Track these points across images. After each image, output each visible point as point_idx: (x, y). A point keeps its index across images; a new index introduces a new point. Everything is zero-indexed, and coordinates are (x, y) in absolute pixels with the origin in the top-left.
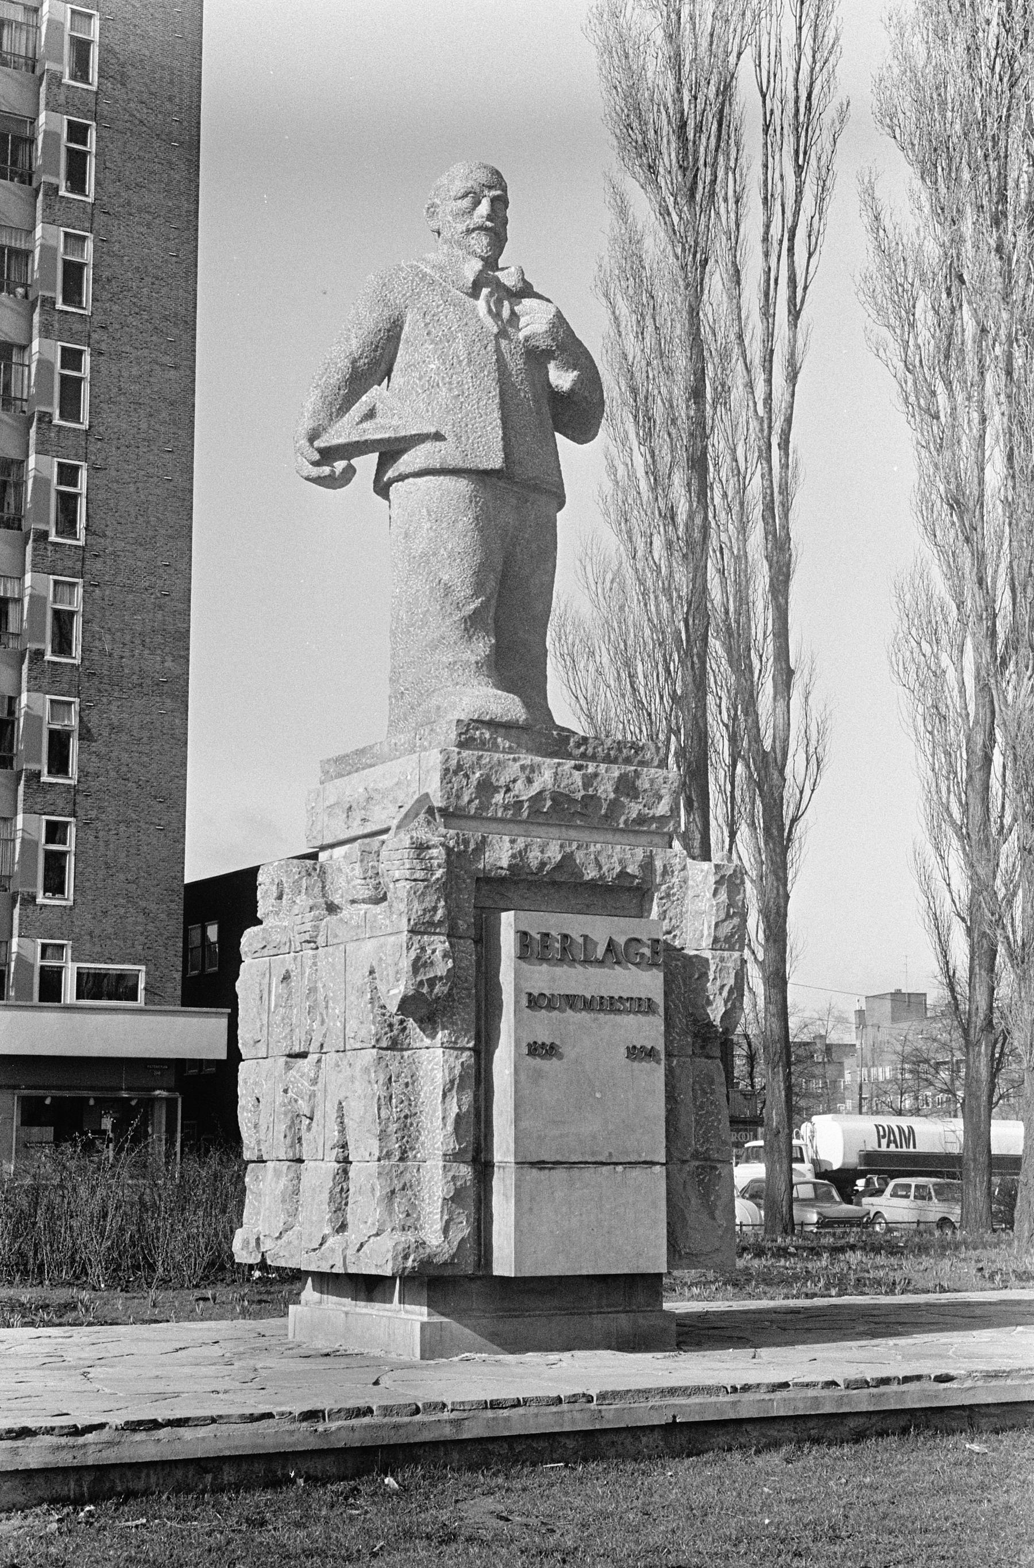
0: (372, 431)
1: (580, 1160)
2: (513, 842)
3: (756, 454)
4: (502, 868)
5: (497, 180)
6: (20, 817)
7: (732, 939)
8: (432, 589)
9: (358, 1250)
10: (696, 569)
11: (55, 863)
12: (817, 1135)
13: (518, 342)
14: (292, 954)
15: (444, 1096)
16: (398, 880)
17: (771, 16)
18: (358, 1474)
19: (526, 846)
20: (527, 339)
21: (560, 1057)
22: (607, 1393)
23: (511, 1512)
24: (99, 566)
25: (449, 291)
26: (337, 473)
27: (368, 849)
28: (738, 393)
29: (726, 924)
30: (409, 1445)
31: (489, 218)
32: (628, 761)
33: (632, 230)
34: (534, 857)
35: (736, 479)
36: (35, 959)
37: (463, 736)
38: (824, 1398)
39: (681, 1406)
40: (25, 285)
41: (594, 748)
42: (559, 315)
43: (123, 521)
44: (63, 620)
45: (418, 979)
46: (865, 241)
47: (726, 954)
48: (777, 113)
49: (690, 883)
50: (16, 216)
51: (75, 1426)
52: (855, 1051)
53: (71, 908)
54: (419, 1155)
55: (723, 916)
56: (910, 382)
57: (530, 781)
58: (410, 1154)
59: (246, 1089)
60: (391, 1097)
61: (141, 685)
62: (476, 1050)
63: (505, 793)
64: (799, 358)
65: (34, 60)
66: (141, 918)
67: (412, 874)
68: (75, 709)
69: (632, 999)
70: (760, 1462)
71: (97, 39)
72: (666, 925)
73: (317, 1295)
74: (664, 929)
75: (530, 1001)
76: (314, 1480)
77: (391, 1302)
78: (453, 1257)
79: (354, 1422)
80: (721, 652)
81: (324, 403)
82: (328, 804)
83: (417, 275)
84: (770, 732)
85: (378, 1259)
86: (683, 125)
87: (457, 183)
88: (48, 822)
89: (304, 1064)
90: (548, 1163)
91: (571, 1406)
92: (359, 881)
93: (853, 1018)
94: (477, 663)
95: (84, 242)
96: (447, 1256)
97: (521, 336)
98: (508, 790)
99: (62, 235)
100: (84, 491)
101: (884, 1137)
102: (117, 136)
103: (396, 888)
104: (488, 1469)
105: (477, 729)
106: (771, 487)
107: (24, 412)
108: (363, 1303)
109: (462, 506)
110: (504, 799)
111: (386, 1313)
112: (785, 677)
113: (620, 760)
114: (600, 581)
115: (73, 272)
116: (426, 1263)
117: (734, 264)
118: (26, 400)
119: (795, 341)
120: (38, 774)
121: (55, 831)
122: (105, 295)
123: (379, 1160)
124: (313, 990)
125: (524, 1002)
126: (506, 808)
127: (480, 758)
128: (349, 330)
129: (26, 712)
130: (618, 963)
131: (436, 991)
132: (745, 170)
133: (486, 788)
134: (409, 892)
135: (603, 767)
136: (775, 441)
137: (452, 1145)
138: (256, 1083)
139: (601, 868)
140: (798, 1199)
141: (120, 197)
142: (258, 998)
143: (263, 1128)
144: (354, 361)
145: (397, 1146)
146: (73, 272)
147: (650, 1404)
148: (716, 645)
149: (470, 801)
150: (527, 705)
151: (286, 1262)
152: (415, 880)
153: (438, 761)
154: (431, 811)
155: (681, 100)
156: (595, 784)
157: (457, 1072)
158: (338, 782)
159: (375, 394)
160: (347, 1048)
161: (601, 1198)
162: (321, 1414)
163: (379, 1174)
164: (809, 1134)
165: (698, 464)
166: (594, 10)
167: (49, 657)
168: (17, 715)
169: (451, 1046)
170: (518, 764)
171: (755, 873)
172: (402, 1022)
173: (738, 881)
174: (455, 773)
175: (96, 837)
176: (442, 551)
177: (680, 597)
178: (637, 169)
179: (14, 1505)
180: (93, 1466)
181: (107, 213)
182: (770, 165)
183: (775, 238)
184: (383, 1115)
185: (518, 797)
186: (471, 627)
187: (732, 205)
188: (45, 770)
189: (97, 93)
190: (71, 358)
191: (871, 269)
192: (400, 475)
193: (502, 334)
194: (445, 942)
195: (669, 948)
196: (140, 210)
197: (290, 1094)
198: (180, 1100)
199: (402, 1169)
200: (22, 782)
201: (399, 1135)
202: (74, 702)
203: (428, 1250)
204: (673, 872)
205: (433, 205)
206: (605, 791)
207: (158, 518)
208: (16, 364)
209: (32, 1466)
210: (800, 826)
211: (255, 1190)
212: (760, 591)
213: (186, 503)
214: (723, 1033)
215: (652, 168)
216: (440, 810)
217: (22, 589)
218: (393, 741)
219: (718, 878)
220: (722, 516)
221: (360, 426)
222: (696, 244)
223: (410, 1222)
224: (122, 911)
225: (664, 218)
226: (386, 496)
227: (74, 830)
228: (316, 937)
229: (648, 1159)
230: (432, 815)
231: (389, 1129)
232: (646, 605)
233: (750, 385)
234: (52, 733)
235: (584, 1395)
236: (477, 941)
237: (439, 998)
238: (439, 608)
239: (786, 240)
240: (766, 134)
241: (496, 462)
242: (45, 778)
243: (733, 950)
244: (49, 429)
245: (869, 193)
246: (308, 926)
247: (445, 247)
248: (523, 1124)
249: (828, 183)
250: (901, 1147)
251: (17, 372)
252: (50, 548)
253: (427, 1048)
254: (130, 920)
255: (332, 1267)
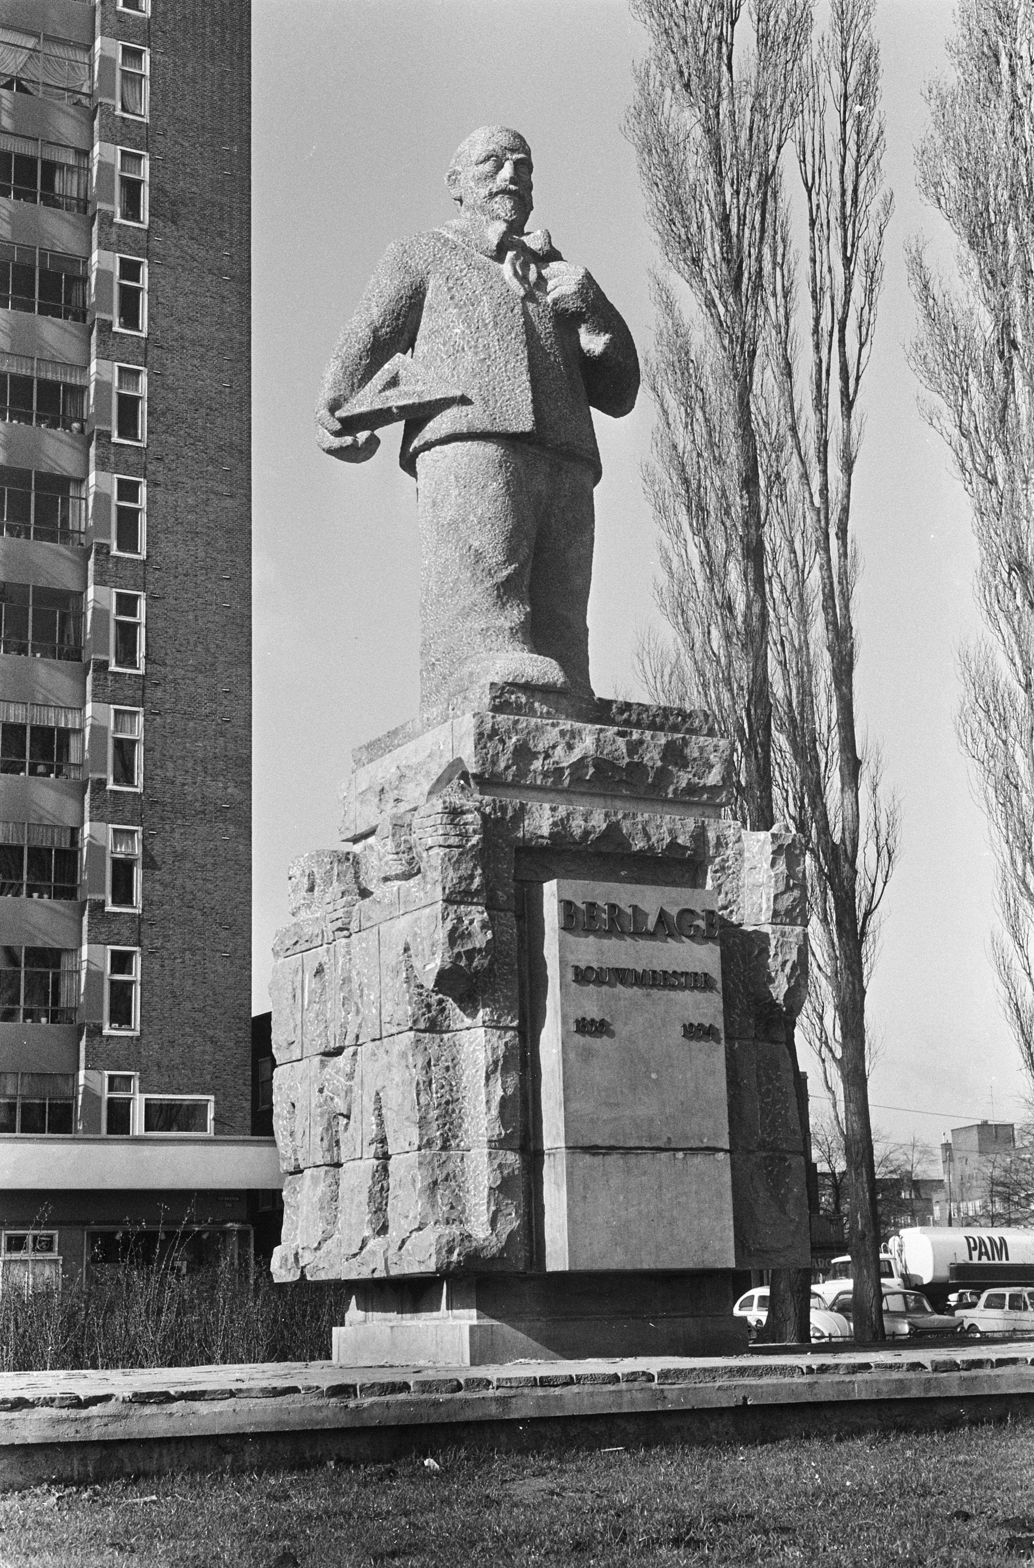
0: (395, 399)
1: (637, 1145)
2: (553, 809)
3: (814, 548)
4: (542, 837)
5: (520, 144)
6: (85, 948)
7: (793, 914)
8: (462, 556)
9: (400, 1248)
10: (756, 658)
11: (121, 993)
12: (906, 1249)
13: (546, 305)
14: (325, 946)
15: (488, 1078)
16: (431, 848)
17: (814, 112)
18: (396, 1455)
19: (568, 815)
20: (555, 302)
21: (611, 1034)
22: (669, 1370)
23: (564, 1489)
24: (159, 694)
25: (473, 255)
26: (360, 443)
27: (400, 822)
28: (793, 486)
29: (786, 896)
30: (451, 1424)
31: (512, 181)
32: (675, 728)
33: (677, 326)
34: (577, 826)
35: (794, 570)
36: (102, 1089)
37: (498, 700)
38: (911, 1380)
39: (751, 1386)
40: (81, 421)
41: (639, 714)
42: (588, 276)
43: (182, 649)
44: (124, 749)
45: (456, 951)
46: (916, 310)
47: (788, 929)
48: (823, 207)
49: (746, 855)
50: (71, 352)
51: (77, 1398)
52: (943, 1187)
53: (138, 1039)
54: (462, 1144)
55: (782, 888)
56: (966, 449)
57: (570, 747)
58: (453, 1143)
59: (281, 1095)
60: (431, 1080)
61: (203, 812)
62: (520, 1030)
63: (545, 759)
64: (853, 450)
65: (86, 202)
66: (209, 1048)
67: (445, 840)
68: (138, 837)
69: (687, 973)
70: (841, 1448)
71: (147, 179)
72: (721, 900)
73: (361, 1314)
74: (720, 904)
75: (576, 975)
76: (344, 1462)
77: (438, 1309)
78: (502, 1250)
79: (389, 1398)
80: (786, 746)
81: (345, 373)
82: (360, 790)
83: (439, 240)
84: (839, 826)
85: (420, 1258)
86: (726, 218)
87: (479, 147)
88: (113, 952)
89: (341, 1061)
90: (602, 1148)
91: (630, 1385)
92: (392, 857)
93: (939, 1152)
94: (511, 629)
95: (138, 377)
96: (495, 1250)
97: (549, 299)
98: (547, 756)
99: (116, 369)
100: (143, 620)
101: (975, 1249)
102: (168, 272)
103: (429, 856)
104: (539, 1453)
105: (512, 693)
106: (830, 577)
107: (82, 544)
108: (409, 1316)
109: (492, 471)
110: (543, 765)
111: (434, 1322)
112: (852, 767)
113: (667, 727)
114: (659, 676)
115: (128, 406)
116: (473, 1257)
117: (785, 357)
118: (83, 533)
119: (849, 431)
120: (102, 904)
121: (121, 963)
122: (160, 428)
123: (419, 1149)
124: (346, 980)
125: (570, 976)
126: (545, 775)
127: (516, 722)
128: (370, 299)
129: (89, 843)
130: (671, 935)
131: (475, 964)
132: (792, 267)
133: (523, 753)
134: (443, 859)
135: (648, 734)
136: (833, 531)
137: (498, 1130)
138: (290, 1088)
139: (649, 839)
140: (888, 1311)
141: (174, 331)
142: (290, 996)
143: (299, 1136)
144: (375, 331)
145: (438, 1133)
146: (128, 406)
147: (718, 1384)
148: (780, 739)
149: (507, 767)
150: (563, 666)
151: (326, 1274)
152: (449, 846)
153: (471, 725)
154: (464, 776)
155: (723, 193)
156: (640, 752)
157: (500, 1052)
158: (369, 767)
159: (397, 362)
160: (384, 1034)
161: (660, 1187)
162: (351, 1390)
163: (420, 1163)
164: (897, 1248)
165: (755, 553)
166: (632, 110)
167: (111, 786)
168: (80, 846)
169: (493, 1025)
170: (557, 729)
171: (829, 970)
172: (440, 1002)
173: (797, 852)
174: (490, 738)
175: (162, 966)
176: (472, 517)
177: (741, 688)
178: (682, 264)
179: (11, 1486)
180: (98, 1441)
181: (160, 347)
182: (818, 259)
183: (825, 330)
184: (422, 1101)
185: (557, 763)
186: (504, 594)
187: (780, 300)
188: (109, 900)
189: (148, 231)
190: (128, 491)
191: (921, 336)
192: (425, 444)
193: (529, 296)
194: (483, 913)
195: (726, 924)
196: (193, 343)
197: (326, 1092)
198: (252, 1232)
199: (444, 1158)
200: (86, 913)
201: (440, 1122)
202: (137, 831)
203: (474, 1244)
204: (727, 844)
205: (454, 172)
206: (652, 758)
207: (217, 645)
208: (72, 497)
209: (30, 1441)
210: (874, 918)
211: (293, 1203)
212: (822, 685)
213: (245, 630)
214: (786, 1013)
215: (696, 261)
216: (474, 776)
217: (83, 720)
218: (425, 716)
219: (775, 848)
220: (782, 609)
221: (383, 394)
222: (744, 334)
223: (456, 1215)
224: (190, 1040)
225: (710, 310)
226: (413, 473)
227: (139, 959)
228: (349, 923)
229: (711, 1144)
230: (467, 782)
231: (429, 1116)
232: (706, 695)
233: (805, 476)
234: (116, 862)
235: (644, 1373)
236: (519, 917)
237: (479, 971)
238: (469, 575)
239: (833, 331)
240: (813, 230)
241: (525, 423)
242: (110, 908)
243: (796, 925)
244: (107, 560)
245: (917, 264)
246: (340, 913)
247: (468, 214)
248: (574, 1106)
249: (876, 274)
250: (994, 1259)
251: (74, 506)
252: (110, 678)
253: (468, 1029)
254: (198, 1049)
255: (373, 1271)
